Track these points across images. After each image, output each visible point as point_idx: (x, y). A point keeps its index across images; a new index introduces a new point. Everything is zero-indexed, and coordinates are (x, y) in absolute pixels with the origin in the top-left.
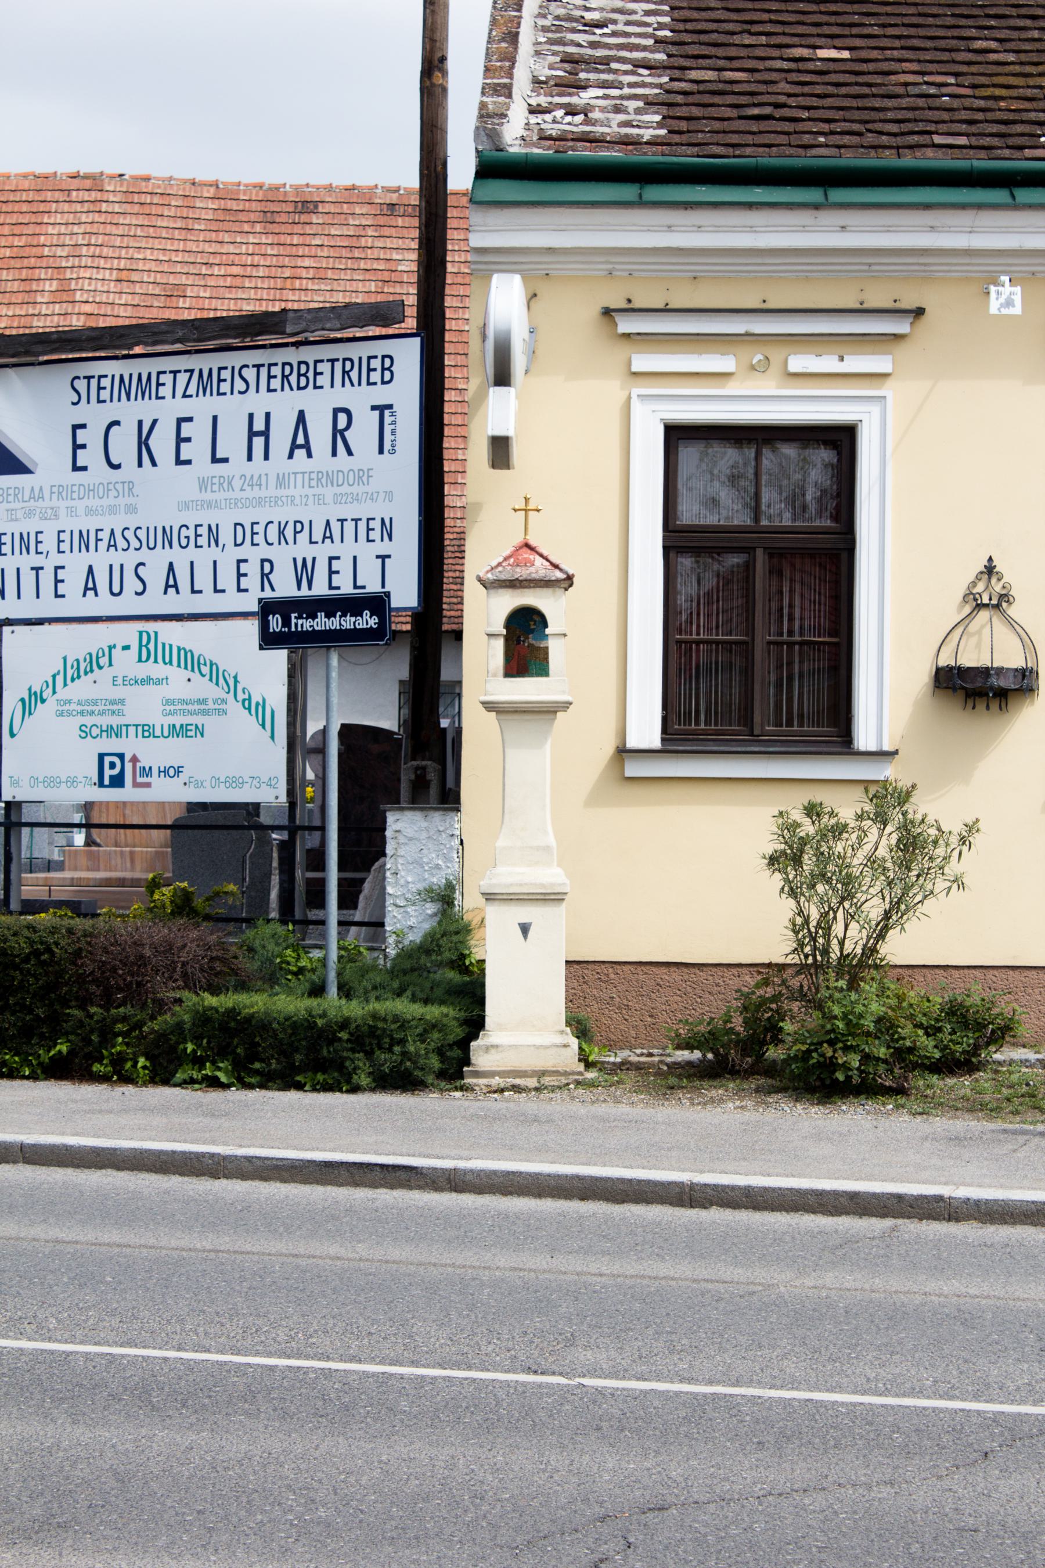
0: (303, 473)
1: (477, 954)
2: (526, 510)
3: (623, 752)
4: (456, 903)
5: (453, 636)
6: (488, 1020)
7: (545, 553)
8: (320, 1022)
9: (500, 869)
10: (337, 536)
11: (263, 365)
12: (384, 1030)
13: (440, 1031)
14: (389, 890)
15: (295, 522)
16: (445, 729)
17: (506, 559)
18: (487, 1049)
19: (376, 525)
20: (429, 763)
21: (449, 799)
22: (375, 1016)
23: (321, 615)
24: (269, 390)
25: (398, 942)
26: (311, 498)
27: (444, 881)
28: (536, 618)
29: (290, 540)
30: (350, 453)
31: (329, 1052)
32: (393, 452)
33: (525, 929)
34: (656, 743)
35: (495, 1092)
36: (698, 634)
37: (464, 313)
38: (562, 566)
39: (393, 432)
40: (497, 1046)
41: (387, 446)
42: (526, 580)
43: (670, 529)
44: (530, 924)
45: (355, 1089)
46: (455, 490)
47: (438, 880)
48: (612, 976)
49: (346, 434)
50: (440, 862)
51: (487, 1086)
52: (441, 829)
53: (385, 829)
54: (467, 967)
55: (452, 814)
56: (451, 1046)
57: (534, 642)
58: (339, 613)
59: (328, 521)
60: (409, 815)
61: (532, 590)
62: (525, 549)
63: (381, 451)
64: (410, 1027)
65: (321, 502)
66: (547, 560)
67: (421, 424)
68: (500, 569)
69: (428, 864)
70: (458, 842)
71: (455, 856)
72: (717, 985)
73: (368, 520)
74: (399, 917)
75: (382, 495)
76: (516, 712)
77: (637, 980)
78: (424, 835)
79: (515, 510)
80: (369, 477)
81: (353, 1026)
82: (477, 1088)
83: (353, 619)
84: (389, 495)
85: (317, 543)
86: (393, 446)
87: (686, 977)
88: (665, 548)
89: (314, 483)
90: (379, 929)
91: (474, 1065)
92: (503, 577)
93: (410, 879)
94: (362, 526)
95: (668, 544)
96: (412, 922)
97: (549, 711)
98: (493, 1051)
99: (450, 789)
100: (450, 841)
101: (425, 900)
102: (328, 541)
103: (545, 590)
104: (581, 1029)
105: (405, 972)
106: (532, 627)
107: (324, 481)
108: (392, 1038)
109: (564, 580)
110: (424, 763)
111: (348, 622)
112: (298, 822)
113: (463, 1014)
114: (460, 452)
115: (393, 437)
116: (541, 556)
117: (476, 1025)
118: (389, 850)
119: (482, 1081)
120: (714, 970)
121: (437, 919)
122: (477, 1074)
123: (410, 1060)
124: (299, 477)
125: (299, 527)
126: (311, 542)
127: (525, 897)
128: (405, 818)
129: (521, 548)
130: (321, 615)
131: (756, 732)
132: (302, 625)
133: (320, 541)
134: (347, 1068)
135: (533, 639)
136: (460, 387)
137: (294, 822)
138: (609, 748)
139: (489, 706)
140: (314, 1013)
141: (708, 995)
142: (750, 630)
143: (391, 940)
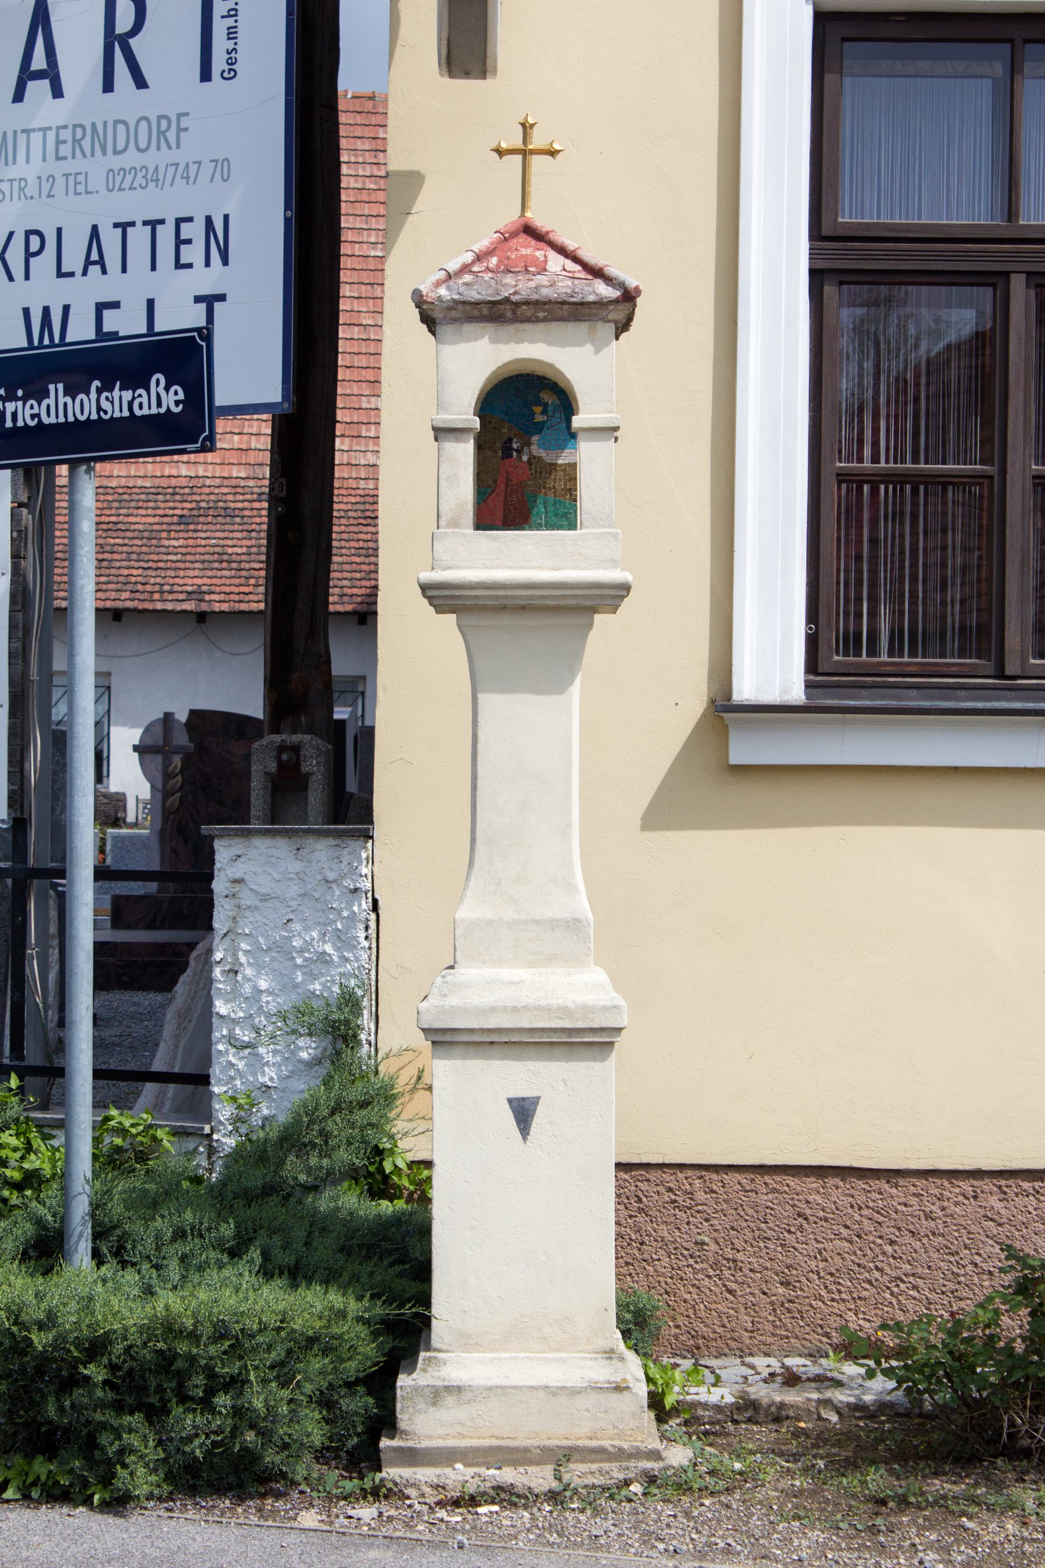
0: (45, 130)
1: (409, 1148)
2: (525, 153)
3: (724, 710)
4: (363, 1037)
5: (356, 618)
6: (437, 1327)
7: (571, 244)
8: (40, 1340)
9: (466, 973)
10: (113, 260)
11: (50, 128)
12: (192, 1359)
13: (326, 1351)
14: (221, 1007)
15: (28, 233)
16: (342, 723)
17: (479, 258)
18: (437, 1394)
19: (194, 231)
20: (307, 737)
21: (350, 811)
22: (170, 1328)
23: (56, 389)
24: (76, 194)
25: (237, 1120)
26: (60, 181)
27: (336, 989)
28: (546, 397)
29: (18, 271)
30: (141, 82)
31: (61, 1409)
32: (230, 74)
33: (523, 1112)
34: (797, 694)
35: (456, 1503)
36: (875, 459)
37: (369, 236)
38: (613, 271)
39: (232, 34)
40: (459, 1389)
41: (219, 63)
42: (527, 303)
43: (825, 232)
44: (536, 1101)
45: (118, 1504)
46: (358, 444)
47: (323, 987)
48: (700, 1196)
49: (133, 42)
50: (328, 948)
51: (436, 1487)
52: (331, 876)
53: (211, 877)
54: (386, 1178)
55: (354, 844)
56: (349, 1385)
57: (542, 453)
58: (96, 383)
59: (95, 229)
60: (261, 844)
61: (541, 326)
62: (523, 238)
63: (206, 75)
64: (254, 1349)
65: (81, 188)
66: (576, 260)
67: (289, 13)
68: (467, 278)
69: (301, 951)
70: (366, 904)
71: (362, 935)
72: (929, 1216)
73: (179, 221)
74: (241, 1065)
75: (207, 168)
76: (504, 608)
77: (755, 1206)
78: (294, 889)
79: (500, 152)
80: (180, 130)
81: (119, 1348)
82: (412, 1492)
83: (127, 395)
84: (223, 168)
85: (72, 274)
86: (231, 62)
87: (861, 1199)
88: (812, 272)
89: (65, 150)
90: (201, 1087)
91: (404, 1432)
92: (473, 295)
93: (263, 985)
94: (166, 235)
95: (821, 265)
96: (269, 1076)
97: (583, 605)
98: (450, 1400)
99: (351, 795)
100: (350, 904)
101: (294, 1032)
102: (95, 270)
103: (571, 326)
104: (636, 1324)
105: (249, 1197)
106: (539, 418)
107: (86, 144)
108: (210, 1373)
109: (616, 301)
110: (296, 738)
111: (117, 403)
112: (31, 861)
113: (379, 1310)
114: (364, 399)
115: (230, 45)
116: (562, 251)
117: (407, 1332)
118: (220, 920)
119: (425, 1474)
120: (921, 1183)
121: (322, 1071)
122: (412, 1457)
123: (252, 1427)
124: (36, 138)
125: (35, 243)
126: (60, 274)
127: (525, 1039)
128: (253, 853)
129: (514, 234)
130: (56, 389)
131: (1008, 671)
132: (14, 415)
133: (79, 271)
134: (103, 1449)
135: (542, 445)
136: (364, 322)
137: (25, 860)
138: (694, 704)
139: (441, 597)
140: (24, 1317)
141: (908, 1238)
142: (995, 448)
143: (224, 1112)
